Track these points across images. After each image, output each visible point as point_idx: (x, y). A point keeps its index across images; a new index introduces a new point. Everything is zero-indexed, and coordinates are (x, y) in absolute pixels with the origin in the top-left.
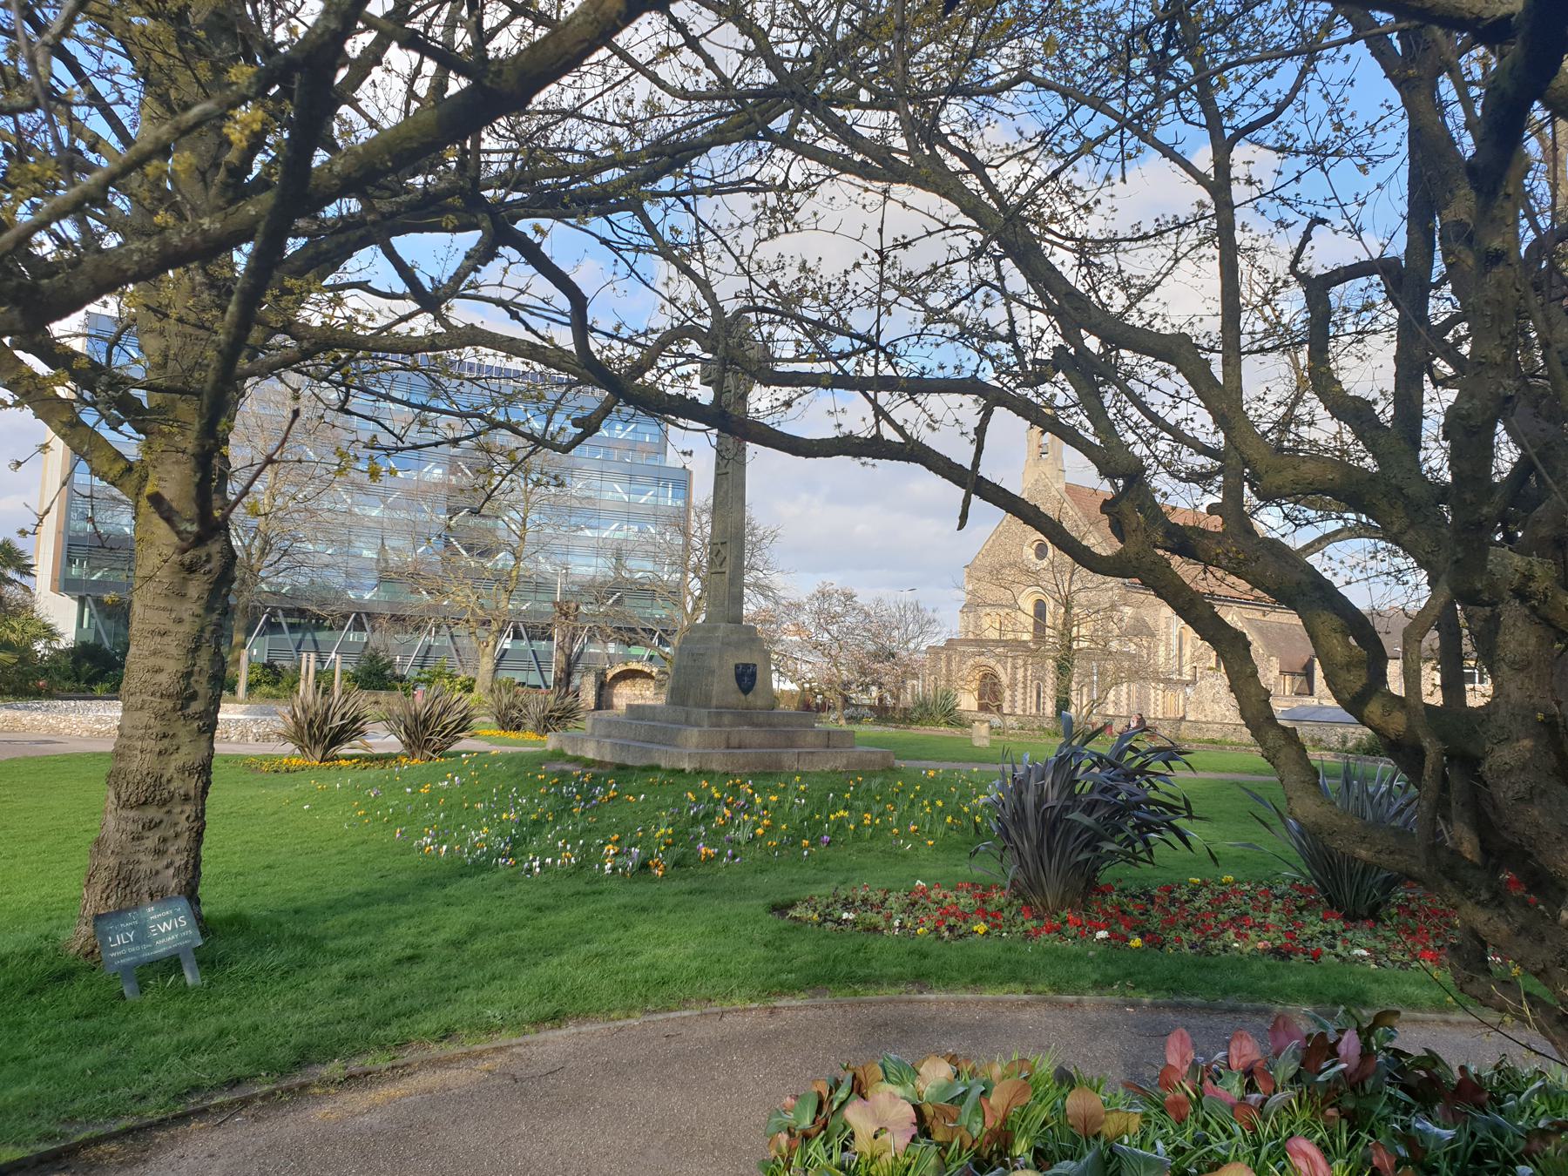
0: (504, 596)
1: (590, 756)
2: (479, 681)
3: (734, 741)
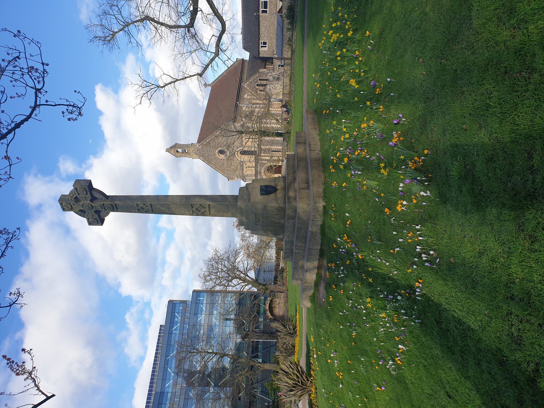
0: (240, 360)
1: (314, 277)
2: (274, 369)
3: (304, 185)
